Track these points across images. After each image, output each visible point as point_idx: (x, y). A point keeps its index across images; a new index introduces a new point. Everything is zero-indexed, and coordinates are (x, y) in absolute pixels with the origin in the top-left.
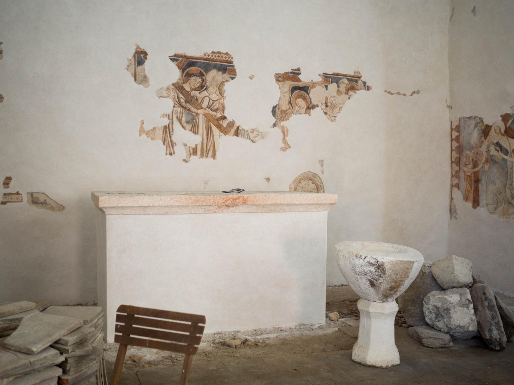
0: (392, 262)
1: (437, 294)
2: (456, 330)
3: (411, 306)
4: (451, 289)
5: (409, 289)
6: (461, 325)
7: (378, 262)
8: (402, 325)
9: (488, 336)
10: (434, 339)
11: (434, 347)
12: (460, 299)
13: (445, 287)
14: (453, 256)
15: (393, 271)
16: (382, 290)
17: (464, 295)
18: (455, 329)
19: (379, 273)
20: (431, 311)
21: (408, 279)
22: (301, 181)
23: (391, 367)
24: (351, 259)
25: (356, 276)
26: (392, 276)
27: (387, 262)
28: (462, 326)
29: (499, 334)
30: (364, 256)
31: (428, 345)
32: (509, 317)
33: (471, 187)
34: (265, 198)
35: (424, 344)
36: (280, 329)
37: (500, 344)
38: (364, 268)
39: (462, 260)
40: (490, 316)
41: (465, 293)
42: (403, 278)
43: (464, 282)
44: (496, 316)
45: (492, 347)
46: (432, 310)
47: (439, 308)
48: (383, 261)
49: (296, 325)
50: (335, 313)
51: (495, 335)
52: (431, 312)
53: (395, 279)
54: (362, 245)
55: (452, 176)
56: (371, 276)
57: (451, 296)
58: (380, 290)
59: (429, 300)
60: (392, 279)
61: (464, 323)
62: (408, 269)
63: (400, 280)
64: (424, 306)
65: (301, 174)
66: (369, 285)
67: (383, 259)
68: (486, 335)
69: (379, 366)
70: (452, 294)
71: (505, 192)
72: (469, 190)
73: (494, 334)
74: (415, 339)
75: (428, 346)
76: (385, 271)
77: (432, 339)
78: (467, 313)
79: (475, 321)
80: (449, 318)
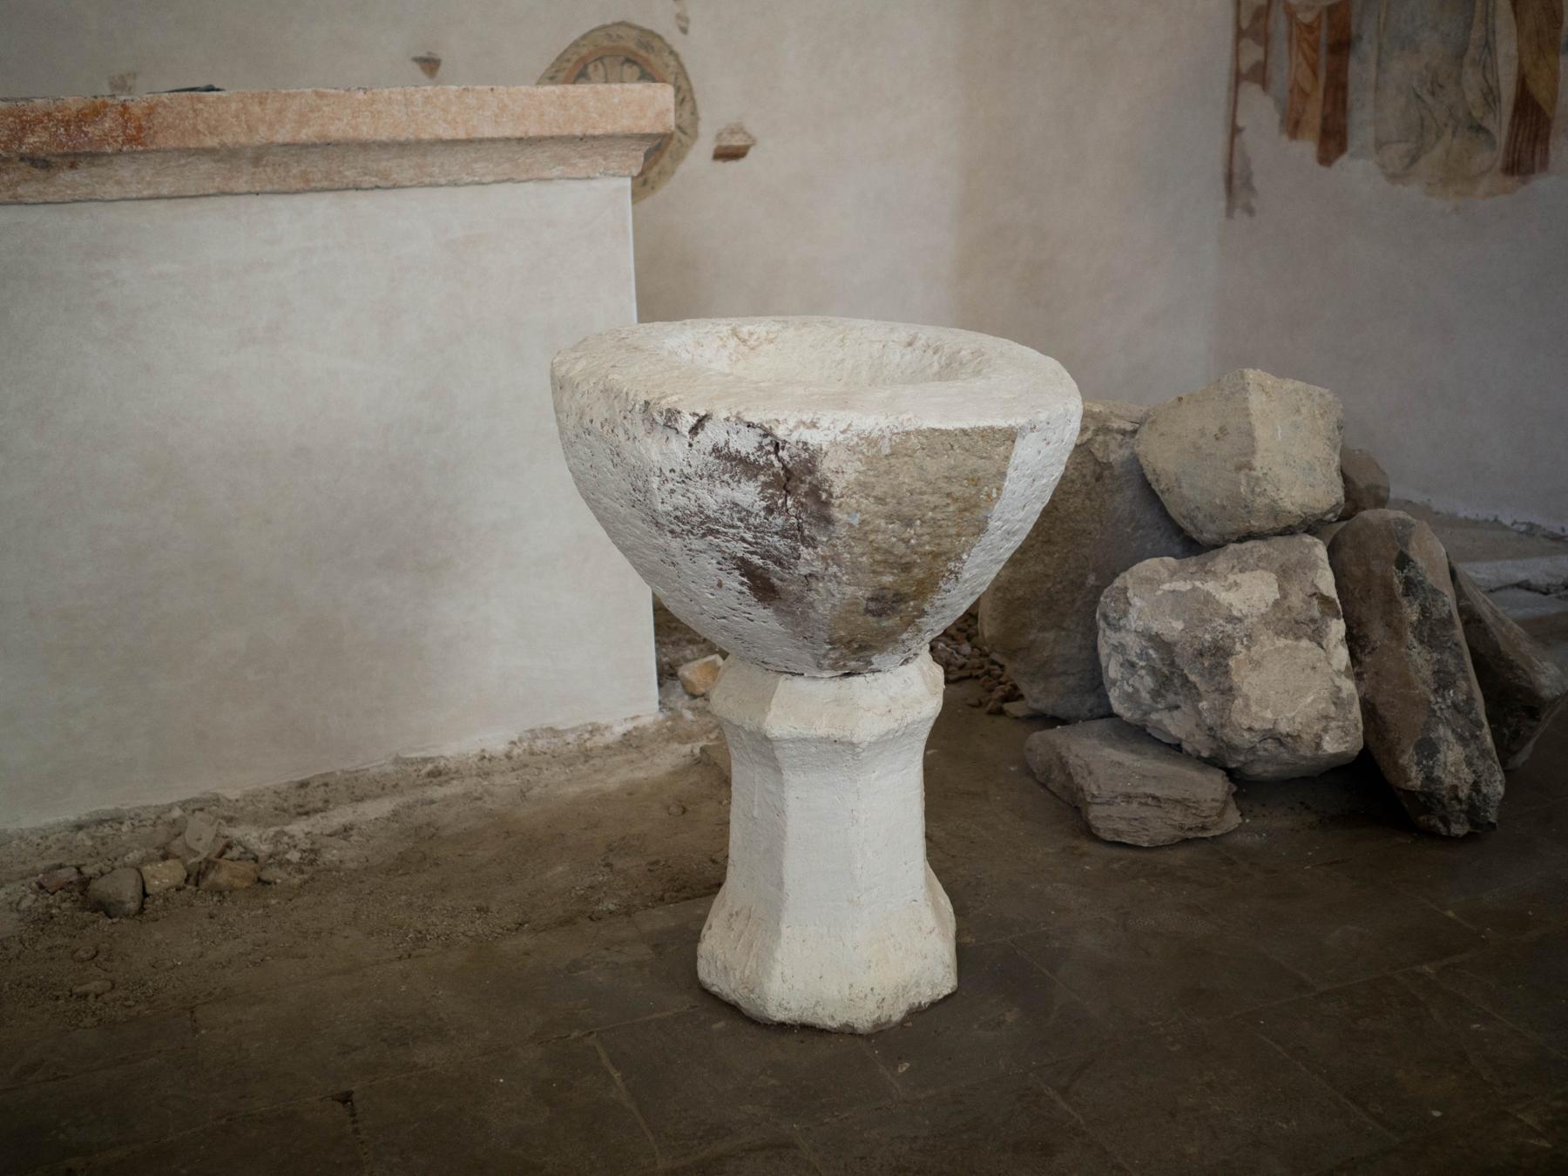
0: (872, 442)
1: (1165, 574)
2: (1254, 753)
3: (1043, 629)
4: (1237, 546)
5: (1032, 546)
6: (1284, 727)
7: (777, 447)
8: (1006, 706)
9: (1413, 775)
10: (1143, 801)
11: (1146, 845)
12: (1278, 596)
13: (1206, 537)
14: (1251, 374)
15: (880, 500)
16: (824, 616)
17: (1299, 571)
18: (1253, 749)
19: (794, 520)
20: (1135, 659)
21: (985, 540)
22: (586, 67)
23: (902, 1023)
24: (622, 437)
25: (661, 541)
26: (876, 531)
27: (834, 443)
28: (1288, 735)
29: (1470, 764)
30: (695, 414)
31: (1117, 832)
32: (1511, 666)
33: (1315, 73)
34: (257, 109)
35: (1098, 829)
36: (430, 767)
37: (1473, 812)
38: (699, 492)
39: (1296, 391)
40: (1429, 673)
41: (1308, 565)
42: (950, 536)
43: (1302, 506)
44: (1460, 675)
45: (1432, 823)
46: (1140, 656)
47: (1175, 644)
48: (810, 441)
49: (515, 738)
50: (707, 663)
51: (1453, 769)
52: (1133, 665)
53: (901, 549)
54: (733, 342)
55: (1240, 34)
56: (743, 540)
57: (1236, 584)
58: (812, 614)
59: (1122, 606)
60: (877, 549)
61: (1298, 720)
62: (975, 481)
63: (931, 552)
64: (1101, 633)
65: (584, 37)
66: (741, 593)
67: (814, 425)
68: (1403, 770)
69: (834, 1024)
70: (1241, 571)
71: (1458, 83)
72: (1307, 86)
73: (1445, 763)
74: (1055, 791)
75: (1117, 839)
76: (827, 504)
77: (1135, 805)
78: (1314, 668)
79: (1351, 704)
80: (1223, 693)
